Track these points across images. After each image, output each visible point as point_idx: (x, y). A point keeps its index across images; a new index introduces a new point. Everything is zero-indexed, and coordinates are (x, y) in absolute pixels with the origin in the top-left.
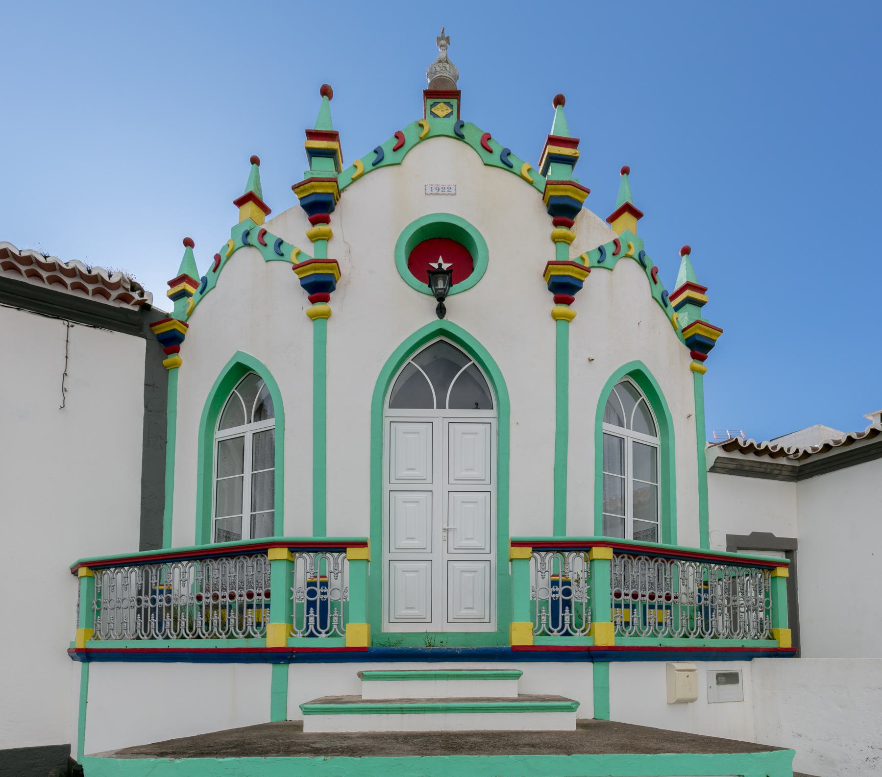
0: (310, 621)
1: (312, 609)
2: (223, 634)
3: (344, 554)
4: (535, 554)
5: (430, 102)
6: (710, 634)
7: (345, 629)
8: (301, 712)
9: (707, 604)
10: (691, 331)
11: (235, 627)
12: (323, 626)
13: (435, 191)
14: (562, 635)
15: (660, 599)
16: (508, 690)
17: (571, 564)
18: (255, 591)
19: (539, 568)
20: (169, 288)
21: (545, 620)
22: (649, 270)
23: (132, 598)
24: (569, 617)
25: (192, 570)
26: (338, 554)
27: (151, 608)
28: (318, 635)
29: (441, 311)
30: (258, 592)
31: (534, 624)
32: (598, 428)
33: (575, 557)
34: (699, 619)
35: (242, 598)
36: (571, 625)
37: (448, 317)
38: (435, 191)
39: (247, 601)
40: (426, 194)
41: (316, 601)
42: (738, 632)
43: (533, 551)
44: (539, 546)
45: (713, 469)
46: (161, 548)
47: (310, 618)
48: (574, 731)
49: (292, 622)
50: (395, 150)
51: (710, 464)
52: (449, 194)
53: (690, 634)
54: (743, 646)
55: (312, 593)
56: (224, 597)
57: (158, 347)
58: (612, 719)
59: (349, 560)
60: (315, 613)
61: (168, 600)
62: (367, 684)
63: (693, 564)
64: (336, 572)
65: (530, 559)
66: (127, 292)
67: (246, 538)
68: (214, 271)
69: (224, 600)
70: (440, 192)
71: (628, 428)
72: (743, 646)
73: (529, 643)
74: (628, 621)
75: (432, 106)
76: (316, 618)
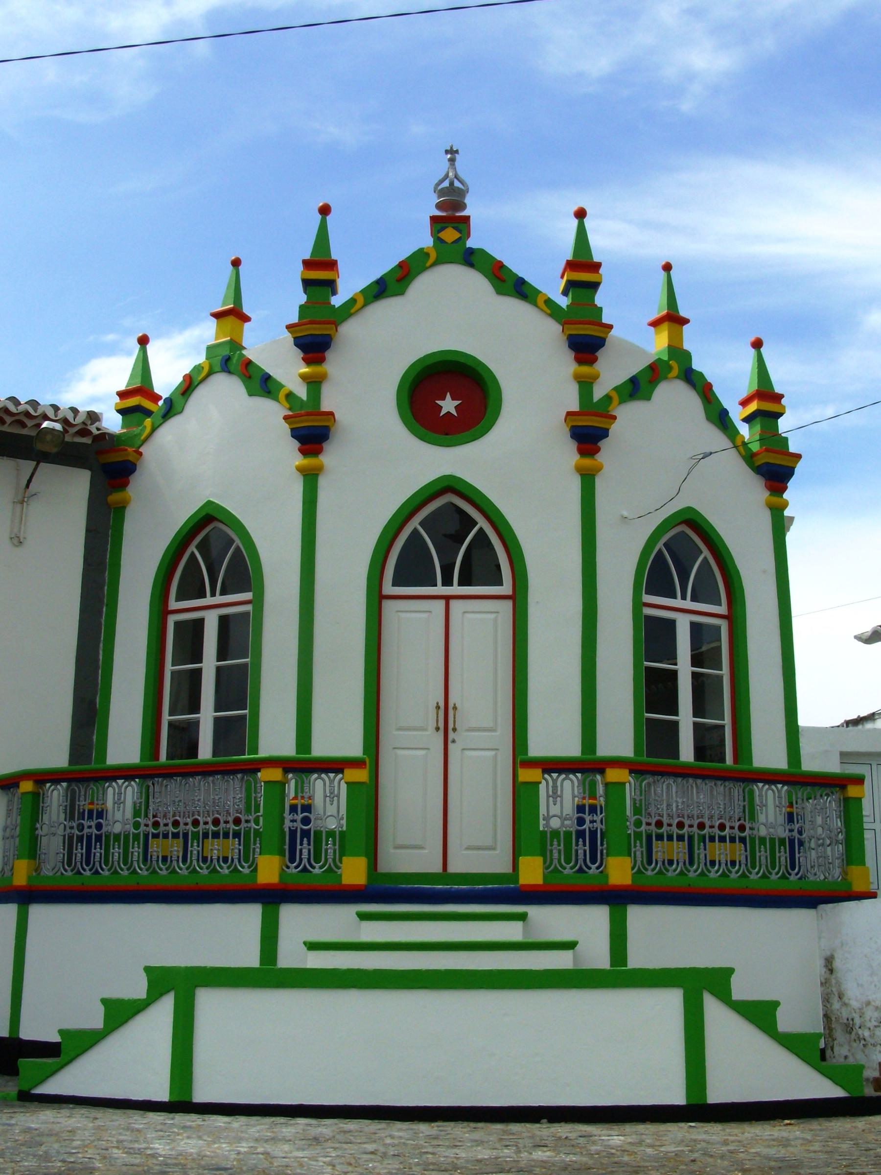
1: (305, 839)
2: (69, 871)
3: (340, 776)
4: (546, 776)
7: (341, 863)
8: (306, 949)
9: (753, 834)
11: (138, 861)
15: (690, 829)
16: (512, 931)
18: (201, 819)
19: (551, 793)
21: (332, 854)
23: (53, 822)
24: (582, 851)
25: (131, 791)
26: (334, 774)
27: (77, 835)
30: (247, 818)
31: (544, 860)
32: (638, 605)
35: (187, 827)
36: (585, 860)
39: (233, 829)
42: (777, 869)
46: (257, 754)
47: (304, 851)
53: (790, 874)
54: (689, 885)
55: (581, 821)
59: (346, 783)
61: (99, 827)
63: (773, 787)
64: (332, 796)
65: (540, 783)
66: (86, 427)
69: (167, 828)
71: (684, 597)
72: (689, 885)
74: (714, 859)
75: (439, 231)
76: (309, 851)
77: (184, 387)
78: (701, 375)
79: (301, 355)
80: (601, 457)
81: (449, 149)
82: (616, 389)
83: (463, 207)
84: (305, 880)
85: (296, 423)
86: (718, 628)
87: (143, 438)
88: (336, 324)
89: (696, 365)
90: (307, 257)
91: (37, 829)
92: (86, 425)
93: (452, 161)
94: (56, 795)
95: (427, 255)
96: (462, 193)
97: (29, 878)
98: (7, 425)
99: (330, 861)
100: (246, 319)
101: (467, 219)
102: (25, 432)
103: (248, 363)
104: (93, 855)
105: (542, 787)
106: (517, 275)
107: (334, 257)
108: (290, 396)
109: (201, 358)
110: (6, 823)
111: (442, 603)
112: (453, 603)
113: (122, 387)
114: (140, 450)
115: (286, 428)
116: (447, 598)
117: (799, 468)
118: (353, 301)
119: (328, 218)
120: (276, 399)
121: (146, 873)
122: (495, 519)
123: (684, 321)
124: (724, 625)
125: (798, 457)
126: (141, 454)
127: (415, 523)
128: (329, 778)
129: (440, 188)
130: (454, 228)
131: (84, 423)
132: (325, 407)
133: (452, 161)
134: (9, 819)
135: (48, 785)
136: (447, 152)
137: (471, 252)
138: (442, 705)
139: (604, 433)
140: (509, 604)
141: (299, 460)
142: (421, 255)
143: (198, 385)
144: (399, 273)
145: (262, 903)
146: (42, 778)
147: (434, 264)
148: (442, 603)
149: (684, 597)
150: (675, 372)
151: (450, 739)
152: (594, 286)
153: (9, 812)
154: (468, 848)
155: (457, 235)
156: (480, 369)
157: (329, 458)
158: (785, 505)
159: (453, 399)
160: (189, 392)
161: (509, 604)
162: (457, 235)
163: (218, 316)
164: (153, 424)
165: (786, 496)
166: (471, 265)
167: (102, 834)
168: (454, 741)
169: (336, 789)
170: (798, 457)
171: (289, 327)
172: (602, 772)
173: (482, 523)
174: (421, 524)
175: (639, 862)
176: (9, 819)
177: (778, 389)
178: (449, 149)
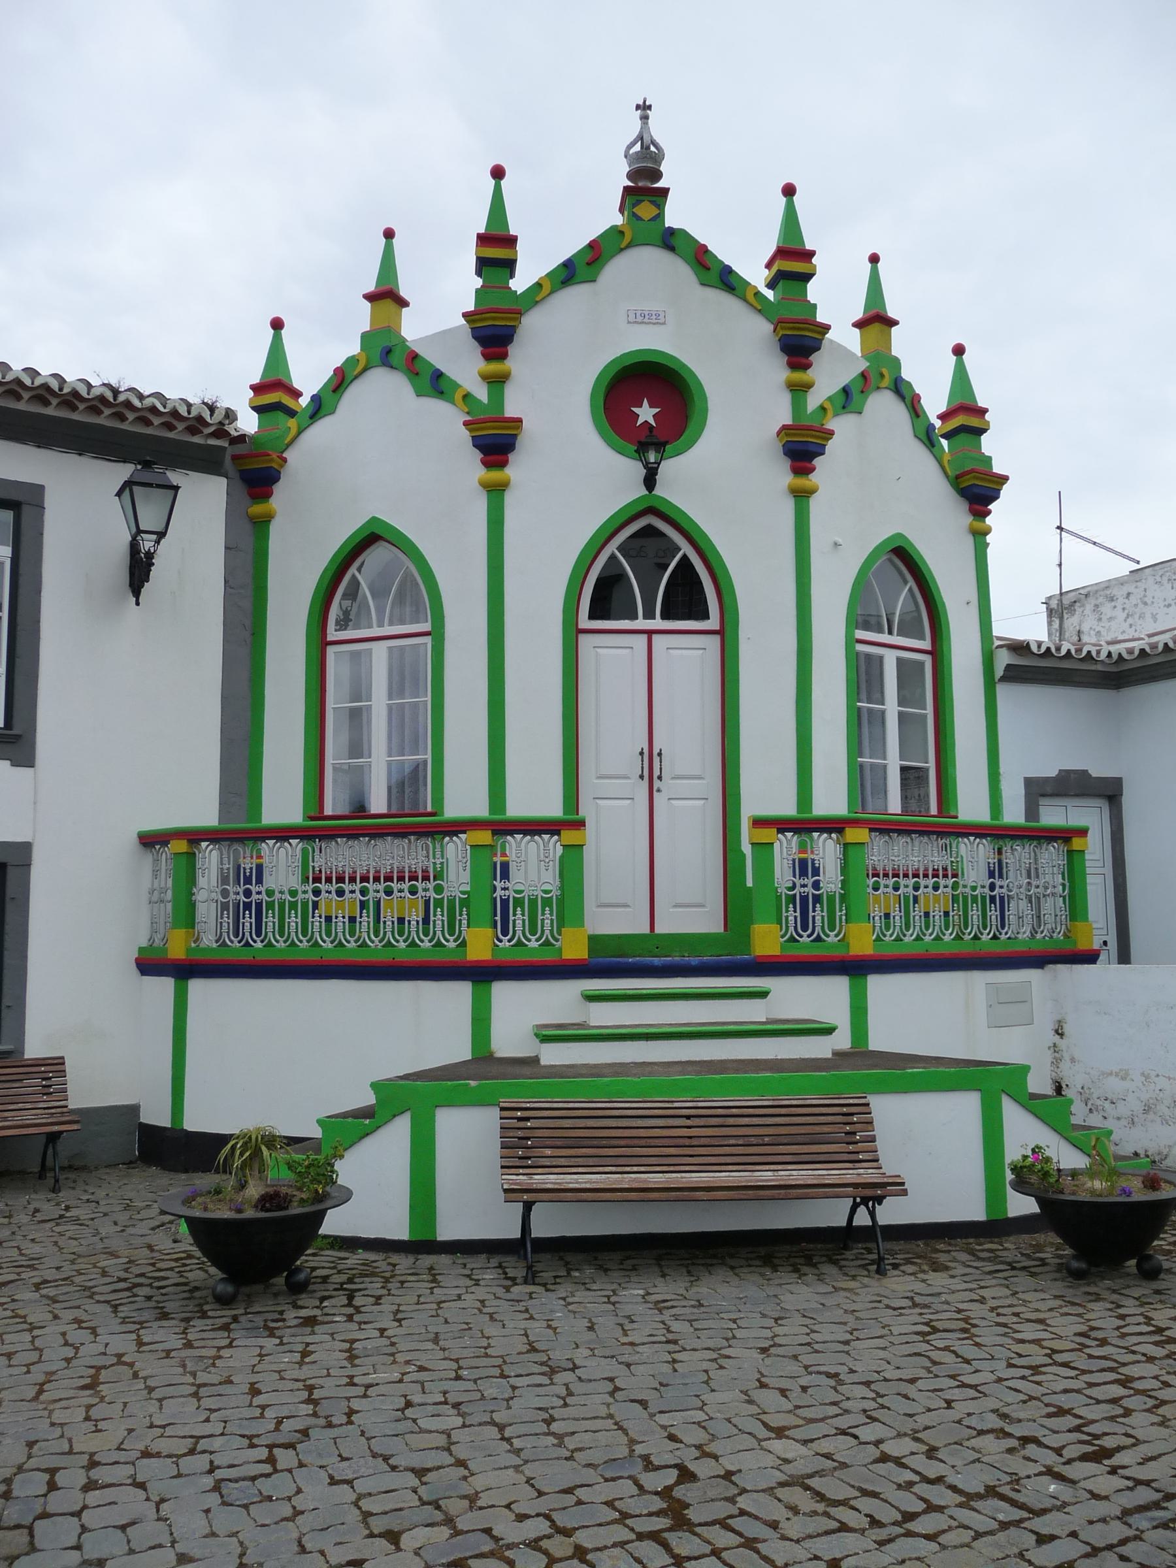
0: (517, 925)
3: (556, 837)
4: (780, 835)
5: (634, 199)
6: (988, 934)
8: (538, 1041)
10: (969, 480)
12: (258, 934)
13: (639, 319)
14: (812, 941)
17: (821, 849)
20: (251, 393)
22: (908, 400)
28: (527, 943)
29: (650, 481)
32: (851, 641)
33: (825, 840)
34: (993, 914)
37: (658, 491)
38: (639, 319)
40: (629, 322)
41: (337, 883)
43: (778, 832)
44: (783, 825)
45: (1005, 679)
48: (829, 1059)
49: (495, 927)
50: (588, 264)
51: (999, 672)
52: (657, 323)
56: (353, 892)
57: (241, 490)
58: (871, 1048)
60: (523, 915)
62: (596, 1007)
67: (429, 809)
68: (334, 391)
70: (646, 320)
71: (890, 633)
73: (776, 951)
75: (634, 205)
77: (335, 382)
78: (909, 384)
79: (479, 349)
80: (815, 478)
81: (641, 103)
82: (829, 399)
83: (657, 175)
84: (520, 956)
85: (478, 430)
86: (921, 664)
87: (288, 439)
88: (519, 313)
89: (906, 374)
90: (482, 231)
91: (194, 894)
92: (224, 425)
93: (645, 118)
94: (211, 858)
95: (622, 233)
96: (658, 157)
97: (188, 950)
98: (127, 422)
99: (547, 932)
100: (403, 303)
101: (664, 192)
102: (149, 431)
103: (413, 357)
104: (264, 924)
105: (777, 845)
106: (722, 262)
107: (512, 232)
108: (467, 396)
109: (354, 348)
110: (153, 885)
111: (644, 637)
112: (655, 637)
113: (256, 379)
114: (284, 455)
115: (465, 435)
116: (650, 633)
117: (1005, 490)
118: (538, 285)
119: (503, 182)
120: (452, 402)
121: (330, 946)
122: (702, 545)
123: (893, 323)
124: (927, 660)
125: (1005, 479)
126: (285, 460)
127: (612, 547)
128: (543, 840)
129: (632, 151)
130: (652, 202)
131: (221, 423)
132: (510, 412)
133: (645, 118)
134: (156, 882)
135: (204, 844)
136: (638, 107)
137: (671, 232)
138: (646, 751)
139: (820, 451)
140: (717, 638)
141: (480, 472)
142: (615, 232)
143: (352, 381)
144: (588, 256)
145: (473, 981)
146: (194, 837)
147: (628, 246)
148: (644, 637)
149: (890, 633)
150: (886, 382)
151: (655, 789)
152: (807, 277)
153: (156, 873)
154: (675, 906)
155: (655, 211)
156: (682, 372)
157: (516, 470)
158: (987, 531)
159: (641, 406)
160: (342, 388)
161: (717, 638)
162: (655, 211)
163: (370, 297)
164: (299, 427)
165: (988, 520)
166: (671, 248)
167: (274, 901)
168: (659, 790)
169: (551, 851)
170: (1005, 479)
171: (466, 315)
172: (840, 831)
173: (686, 549)
174: (620, 549)
175: (877, 929)
176: (156, 882)
177: (981, 403)
178: (641, 103)
